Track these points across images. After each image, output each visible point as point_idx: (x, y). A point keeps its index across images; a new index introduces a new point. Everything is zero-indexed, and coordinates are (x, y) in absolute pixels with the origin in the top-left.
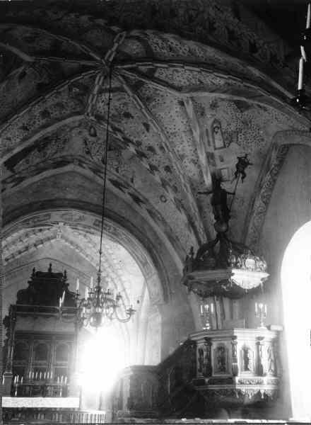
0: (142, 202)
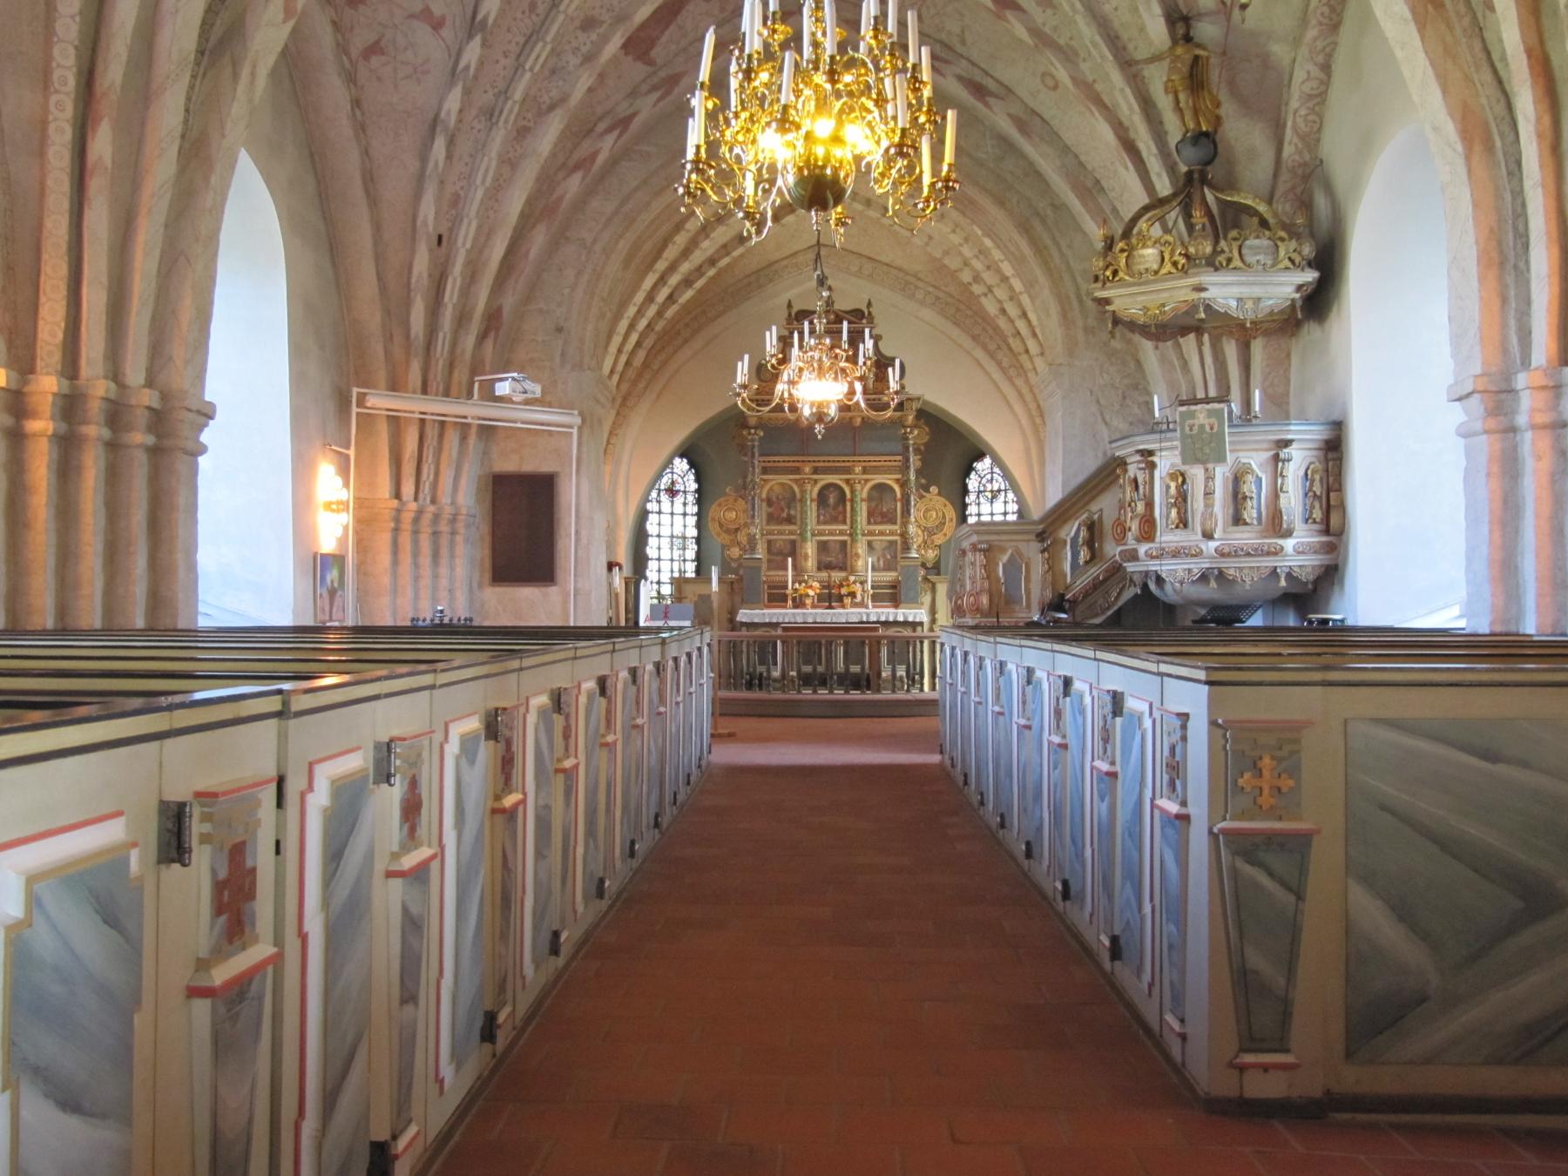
0: (996, 96)
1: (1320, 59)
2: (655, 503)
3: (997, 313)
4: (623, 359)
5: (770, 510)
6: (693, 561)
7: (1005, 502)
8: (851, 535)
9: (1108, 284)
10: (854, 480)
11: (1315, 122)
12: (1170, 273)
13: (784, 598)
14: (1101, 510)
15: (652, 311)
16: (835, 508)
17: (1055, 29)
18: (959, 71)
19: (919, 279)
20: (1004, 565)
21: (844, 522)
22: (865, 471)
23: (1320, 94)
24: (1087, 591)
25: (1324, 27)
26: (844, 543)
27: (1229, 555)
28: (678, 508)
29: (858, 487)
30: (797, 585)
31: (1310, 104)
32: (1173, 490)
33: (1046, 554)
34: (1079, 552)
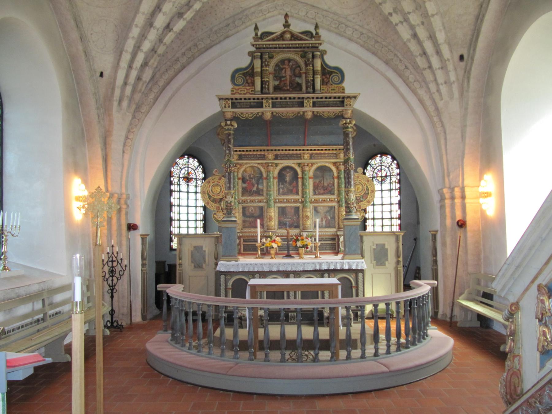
2: (176, 186)
3: (409, 37)
4: (134, 74)
5: (245, 185)
6: (201, 221)
7: (390, 183)
8: (302, 202)
10: (304, 163)
13: (255, 249)
15: (152, 35)
16: (290, 184)
19: (348, 20)
21: (297, 193)
22: (311, 157)
26: (297, 208)
28: (192, 188)
29: (307, 168)
30: (264, 240)
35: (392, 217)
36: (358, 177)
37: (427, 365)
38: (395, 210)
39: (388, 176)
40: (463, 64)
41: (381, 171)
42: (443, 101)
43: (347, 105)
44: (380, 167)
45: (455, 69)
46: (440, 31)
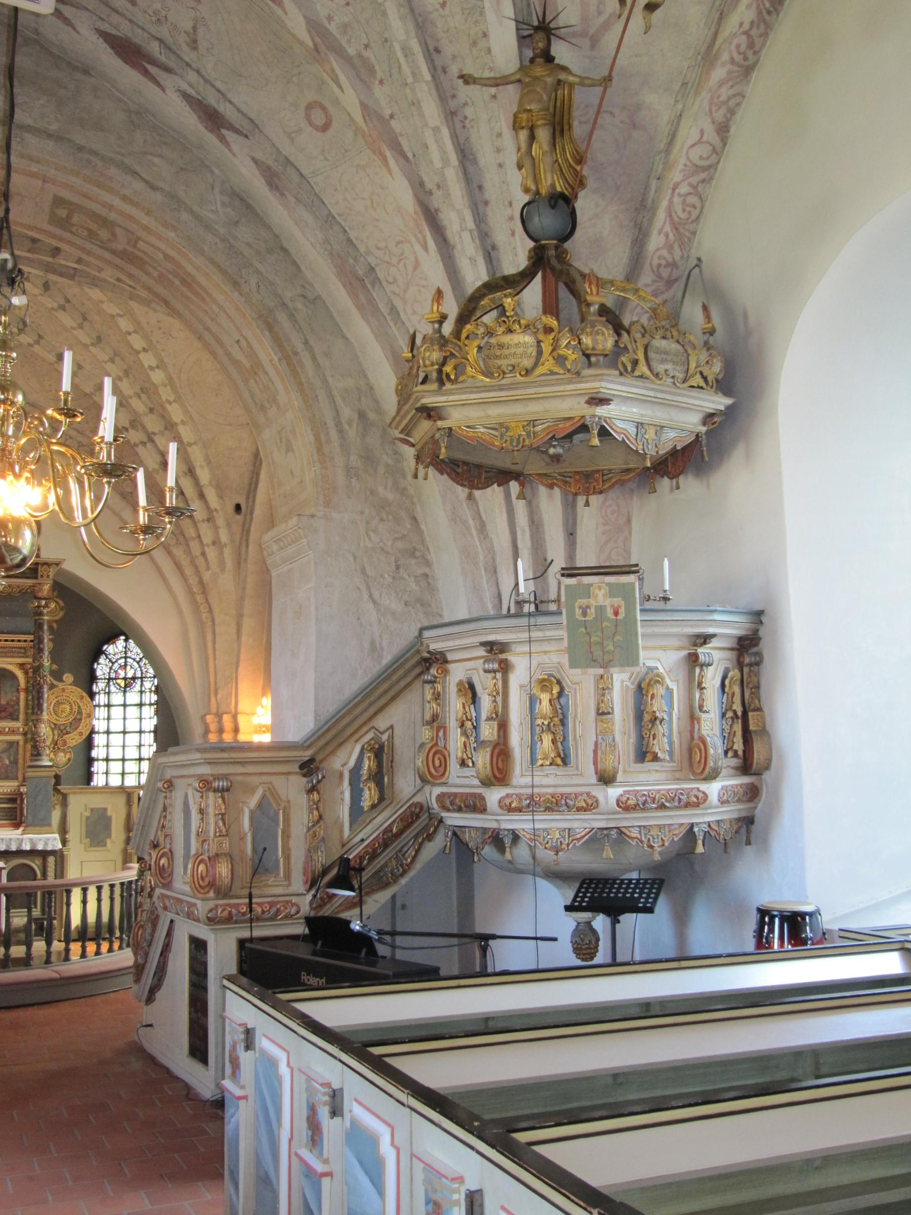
1: (720, 115)
7: (141, 692)
9: (448, 386)
11: (694, 207)
12: (552, 373)
14: (392, 727)
17: (345, 28)
18: (185, 87)
20: (251, 812)
23: (710, 167)
24: (375, 850)
25: (736, 68)
27: (635, 808)
31: (694, 180)
32: (544, 706)
33: (315, 796)
34: (362, 790)
35: (142, 756)
36: (64, 690)
37: (118, 973)
38: (147, 743)
39: (138, 678)
40: (239, 518)
41: (125, 669)
42: (210, 572)
43: (42, 576)
44: (123, 660)
45: (229, 525)
46: (202, 467)
